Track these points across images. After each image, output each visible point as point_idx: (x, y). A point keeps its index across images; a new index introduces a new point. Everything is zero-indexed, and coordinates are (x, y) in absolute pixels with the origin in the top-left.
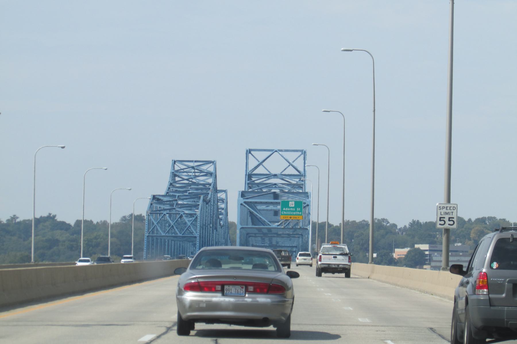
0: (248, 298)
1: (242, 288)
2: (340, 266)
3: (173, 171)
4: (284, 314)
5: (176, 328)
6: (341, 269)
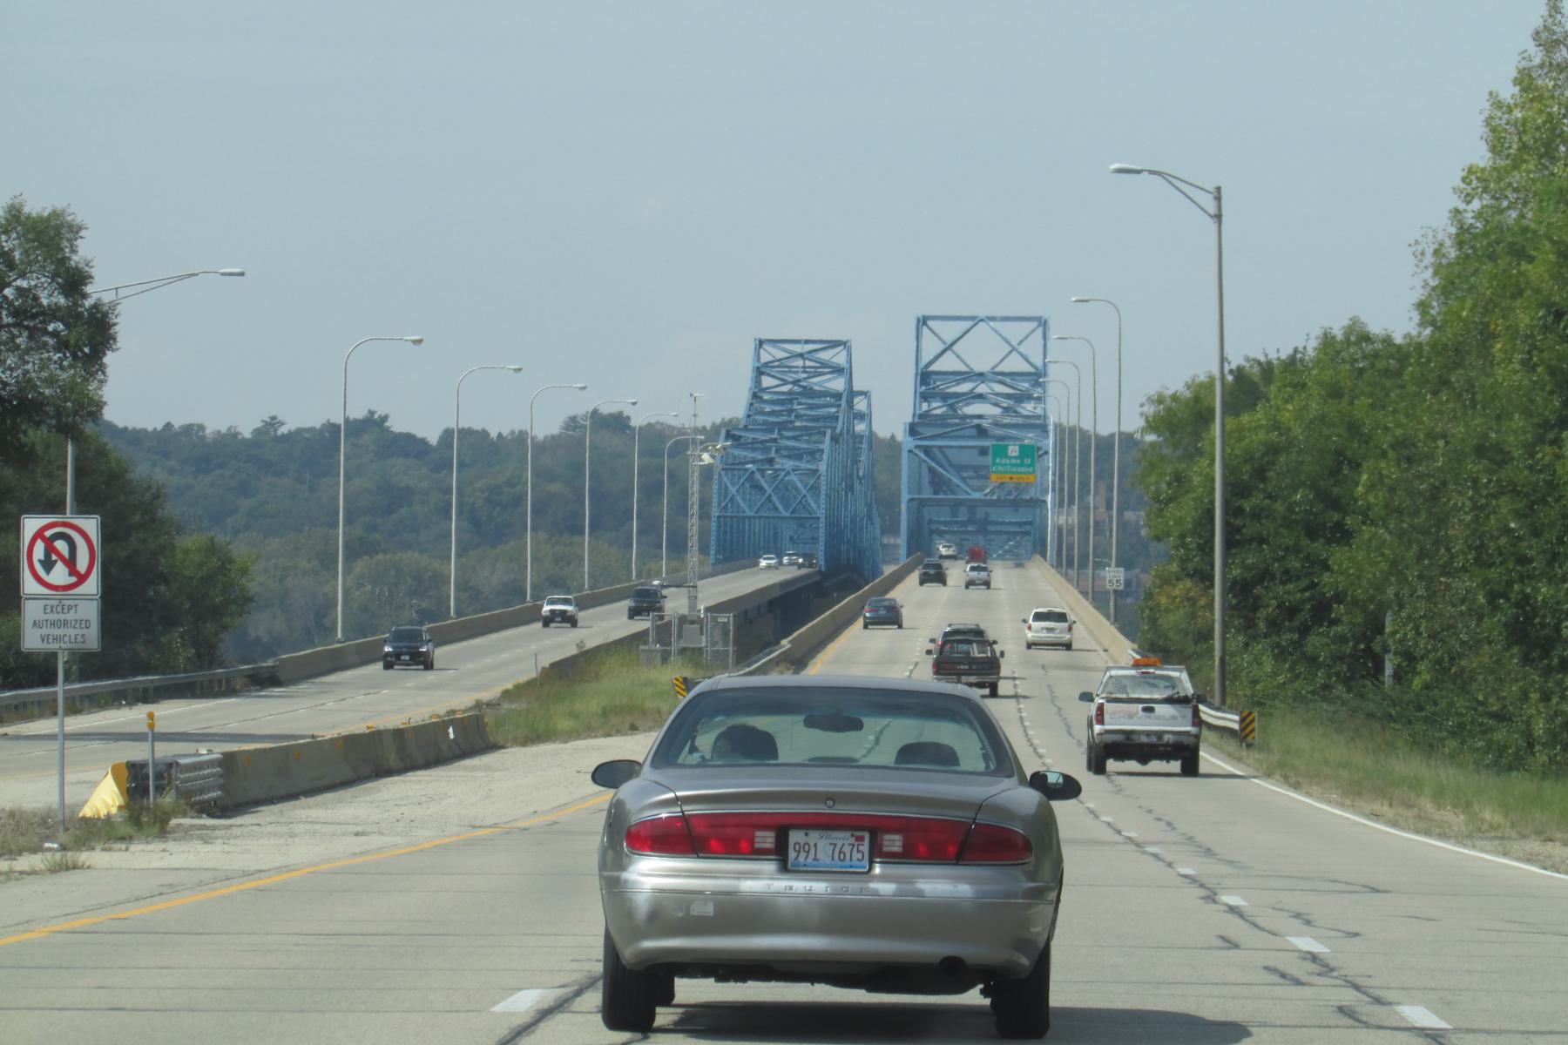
0: (883, 878)
1: (860, 839)
2: (1166, 738)
3: (759, 365)
4: (1022, 945)
5: (594, 998)
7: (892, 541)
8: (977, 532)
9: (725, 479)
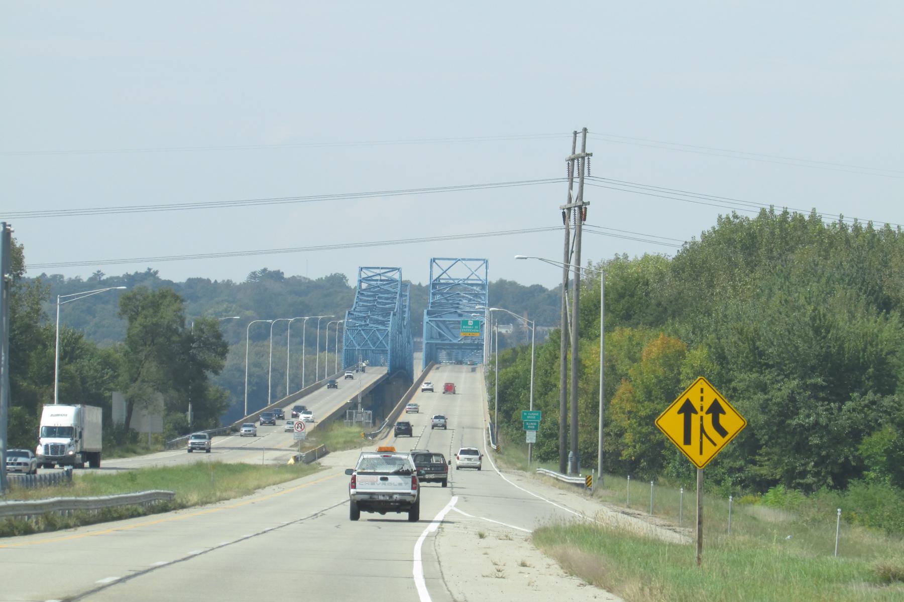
2: (395, 496)
6: (397, 504)
7: (419, 340)
8: (458, 349)
9: (348, 333)
